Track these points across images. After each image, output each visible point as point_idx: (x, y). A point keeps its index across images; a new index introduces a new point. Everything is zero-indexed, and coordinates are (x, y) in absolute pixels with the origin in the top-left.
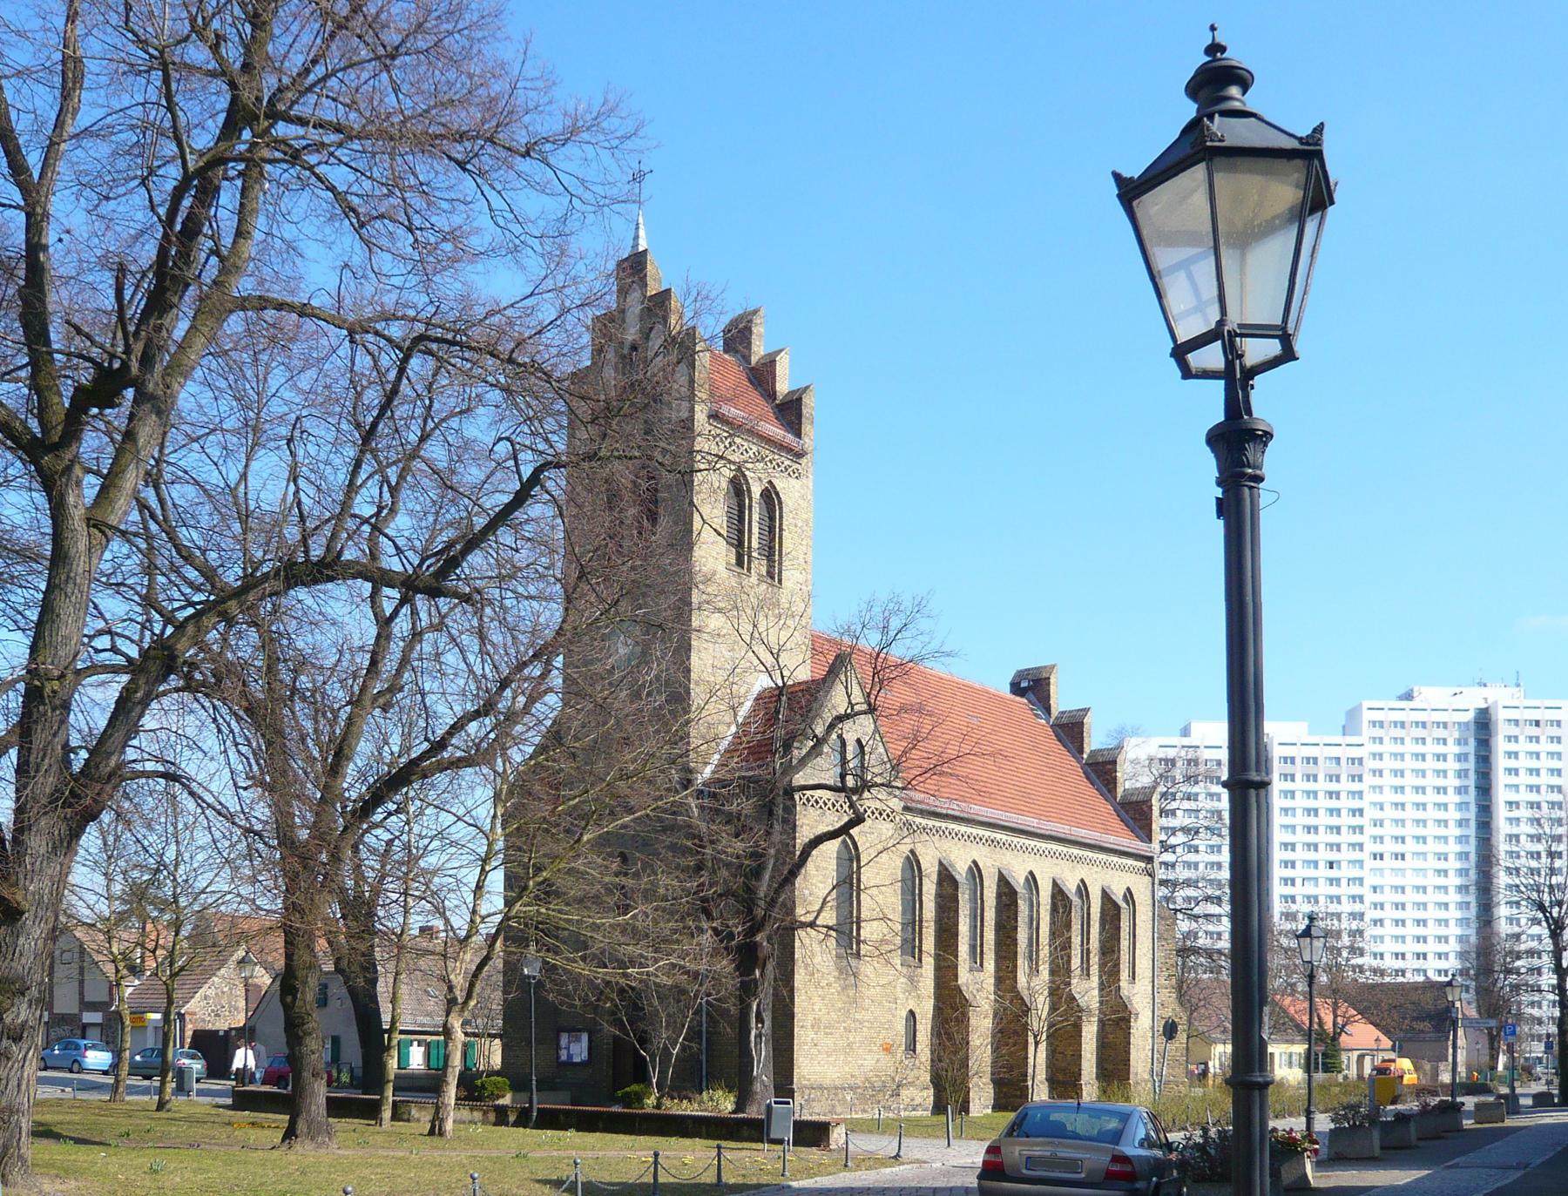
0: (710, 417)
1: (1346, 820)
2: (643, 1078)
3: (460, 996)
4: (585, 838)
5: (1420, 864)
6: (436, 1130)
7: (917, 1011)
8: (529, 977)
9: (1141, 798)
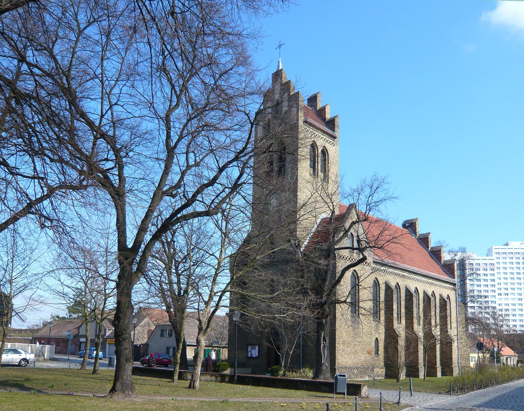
0: (304, 122)
1: (489, 283)
2: (278, 363)
3: (204, 326)
5: (513, 297)
6: (192, 386)
7: (379, 338)
8: (235, 321)
9: (450, 263)
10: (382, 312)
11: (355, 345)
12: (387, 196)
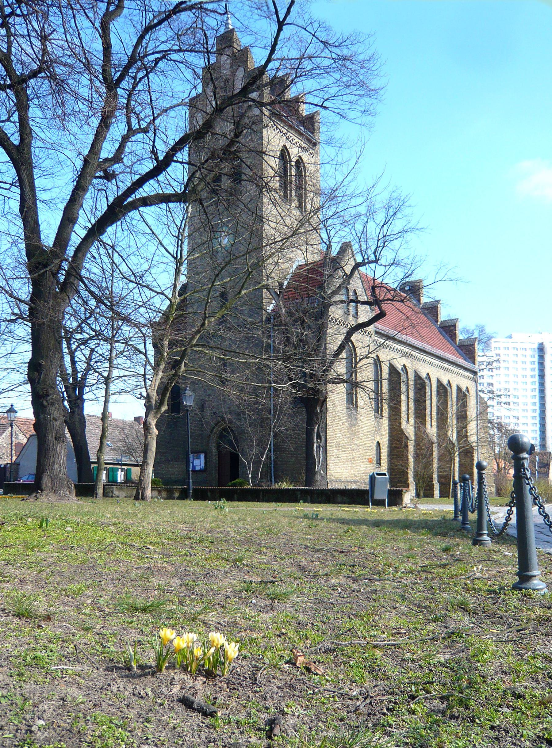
4: (243, 292)
7: (381, 442)
9: (469, 343)
10: (385, 407)
11: (353, 450)
12: (409, 226)
